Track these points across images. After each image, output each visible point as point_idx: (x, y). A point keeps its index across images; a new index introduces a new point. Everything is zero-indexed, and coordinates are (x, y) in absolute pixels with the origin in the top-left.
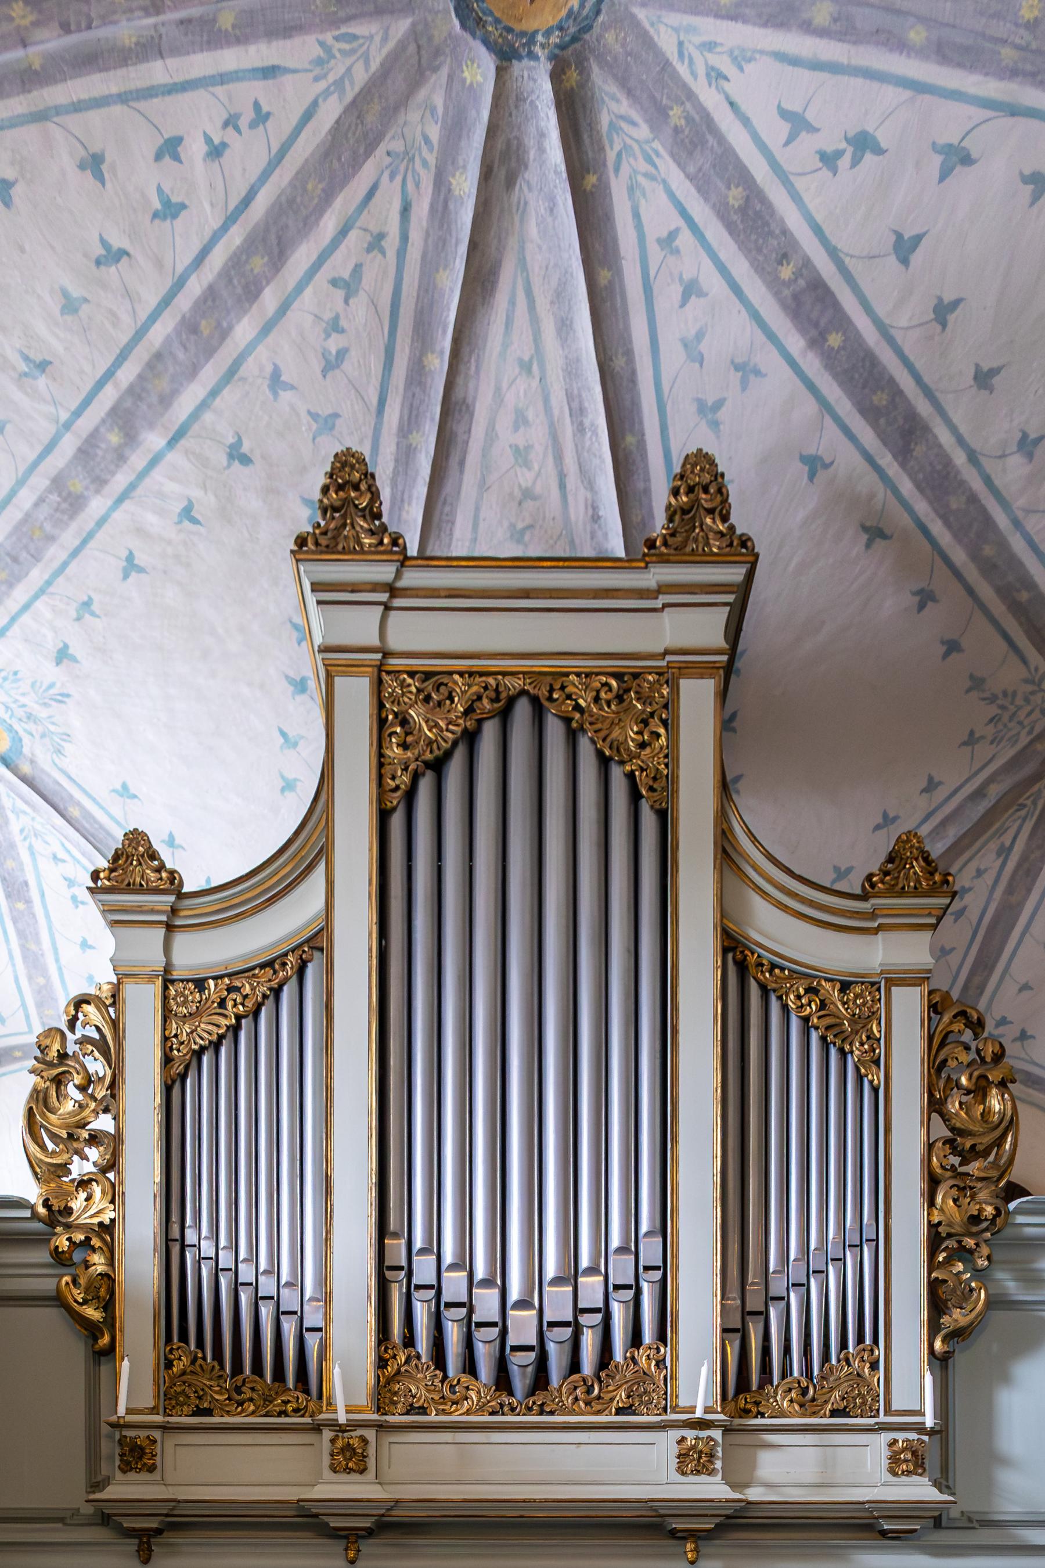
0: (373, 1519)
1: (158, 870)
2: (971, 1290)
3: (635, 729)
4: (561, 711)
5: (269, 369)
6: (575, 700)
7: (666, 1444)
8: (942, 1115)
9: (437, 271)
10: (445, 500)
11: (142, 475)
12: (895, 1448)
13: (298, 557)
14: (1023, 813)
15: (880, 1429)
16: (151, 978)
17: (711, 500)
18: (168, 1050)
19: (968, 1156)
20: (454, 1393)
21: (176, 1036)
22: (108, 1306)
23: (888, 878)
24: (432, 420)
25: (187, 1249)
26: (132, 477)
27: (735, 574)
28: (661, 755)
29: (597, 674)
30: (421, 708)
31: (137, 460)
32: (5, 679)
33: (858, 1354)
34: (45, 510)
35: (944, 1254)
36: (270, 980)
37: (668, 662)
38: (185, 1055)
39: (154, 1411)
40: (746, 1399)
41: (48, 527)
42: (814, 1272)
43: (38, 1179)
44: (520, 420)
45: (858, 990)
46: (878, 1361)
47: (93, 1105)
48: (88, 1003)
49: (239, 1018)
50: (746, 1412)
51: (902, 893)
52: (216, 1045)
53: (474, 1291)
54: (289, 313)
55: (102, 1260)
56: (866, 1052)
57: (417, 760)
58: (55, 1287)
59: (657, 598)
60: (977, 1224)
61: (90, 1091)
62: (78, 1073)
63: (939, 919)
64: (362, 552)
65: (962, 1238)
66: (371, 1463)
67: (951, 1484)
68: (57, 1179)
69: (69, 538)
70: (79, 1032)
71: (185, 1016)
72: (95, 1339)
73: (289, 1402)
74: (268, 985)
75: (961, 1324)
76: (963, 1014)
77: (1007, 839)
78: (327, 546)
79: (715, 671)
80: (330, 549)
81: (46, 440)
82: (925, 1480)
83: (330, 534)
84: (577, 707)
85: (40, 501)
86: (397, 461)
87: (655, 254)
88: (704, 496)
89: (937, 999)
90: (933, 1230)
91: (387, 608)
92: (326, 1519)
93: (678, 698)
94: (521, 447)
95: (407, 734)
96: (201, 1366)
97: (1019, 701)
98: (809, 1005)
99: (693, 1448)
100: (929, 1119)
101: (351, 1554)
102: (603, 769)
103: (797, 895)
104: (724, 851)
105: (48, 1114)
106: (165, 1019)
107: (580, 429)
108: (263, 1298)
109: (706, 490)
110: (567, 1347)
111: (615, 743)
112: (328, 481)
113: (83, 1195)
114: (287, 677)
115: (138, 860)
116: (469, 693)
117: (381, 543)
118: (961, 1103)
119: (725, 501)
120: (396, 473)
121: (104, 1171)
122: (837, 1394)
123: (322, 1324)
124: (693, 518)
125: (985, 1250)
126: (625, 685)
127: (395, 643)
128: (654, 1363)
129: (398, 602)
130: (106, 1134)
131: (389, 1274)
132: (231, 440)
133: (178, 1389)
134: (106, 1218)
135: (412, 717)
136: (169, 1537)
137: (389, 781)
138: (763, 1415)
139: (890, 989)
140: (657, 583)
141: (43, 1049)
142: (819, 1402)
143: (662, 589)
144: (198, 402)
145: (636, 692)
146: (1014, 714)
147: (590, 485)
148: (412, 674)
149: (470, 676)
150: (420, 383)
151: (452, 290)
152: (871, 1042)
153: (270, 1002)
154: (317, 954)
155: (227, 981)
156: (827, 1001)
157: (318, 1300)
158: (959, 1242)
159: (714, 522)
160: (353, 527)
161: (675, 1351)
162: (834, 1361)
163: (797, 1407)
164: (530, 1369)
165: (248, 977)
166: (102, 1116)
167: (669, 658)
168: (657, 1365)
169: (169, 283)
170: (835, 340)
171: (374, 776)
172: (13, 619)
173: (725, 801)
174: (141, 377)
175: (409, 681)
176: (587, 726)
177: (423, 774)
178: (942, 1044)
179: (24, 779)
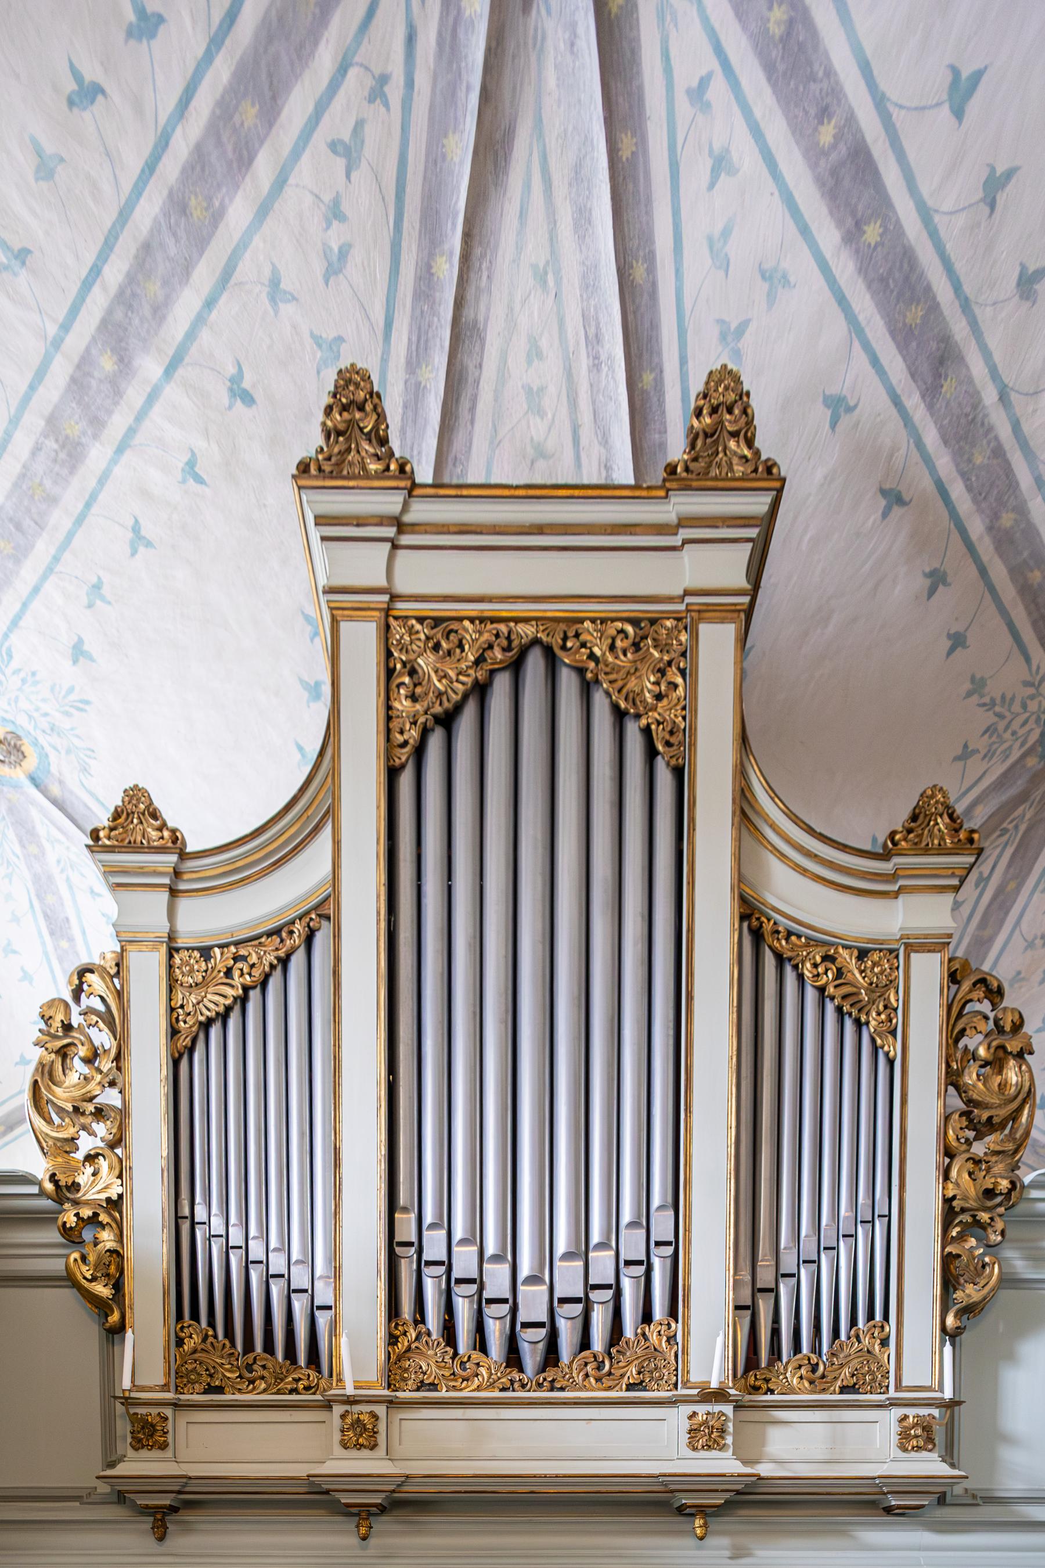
0: (383, 1495)
3: (652, 679)
4: (576, 661)
5: (267, 272)
6: (590, 648)
7: (678, 1419)
8: (957, 1087)
9: (446, 136)
12: (905, 1424)
13: (302, 483)
15: (891, 1405)
16: (156, 943)
17: (736, 421)
18: (174, 1020)
19: (983, 1129)
20: (465, 1369)
21: (182, 1007)
22: (118, 1286)
23: (911, 836)
25: (197, 1226)
26: (130, 420)
27: (757, 504)
29: (613, 620)
30: (431, 657)
31: (135, 395)
33: (868, 1331)
35: (958, 1229)
36: (277, 949)
37: (687, 605)
38: (191, 1027)
39: (165, 1388)
40: (756, 1375)
41: (48, 483)
42: (825, 1248)
43: (44, 1154)
44: (535, 353)
46: (888, 1337)
47: (98, 1077)
48: (92, 971)
49: (246, 989)
50: (756, 1389)
51: (926, 851)
52: (224, 1017)
53: (485, 1266)
54: (286, 188)
56: (882, 1022)
57: (426, 713)
58: (64, 1268)
59: (676, 534)
60: (991, 1199)
61: (96, 1065)
62: (83, 1045)
63: (962, 882)
64: (368, 476)
65: (976, 1213)
66: (381, 1438)
67: (955, 1461)
68: (65, 1155)
69: (72, 499)
71: (191, 986)
72: (107, 1316)
73: (300, 1379)
74: (275, 954)
75: (974, 1299)
76: (983, 981)
78: (332, 472)
79: (735, 615)
80: (331, 476)
82: (934, 1456)
83: (334, 460)
84: (592, 656)
85: (37, 449)
86: (405, 407)
87: (683, 107)
88: (728, 417)
89: (957, 966)
90: (947, 1207)
91: (395, 547)
92: (338, 1495)
94: (535, 389)
95: (415, 685)
96: (212, 1343)
97: (1017, 707)
98: (826, 973)
99: (705, 1423)
100: (946, 1091)
101: (363, 1530)
103: (816, 856)
104: (743, 812)
105: (54, 1087)
106: (171, 989)
109: (730, 411)
110: (579, 1322)
111: (631, 695)
113: (89, 1170)
114: (301, 681)
115: (139, 818)
116: (479, 642)
118: (978, 1075)
119: (750, 423)
121: (112, 1145)
122: (846, 1371)
123: (331, 1303)
124: (716, 442)
125: (999, 1225)
126: (642, 632)
127: (402, 587)
128: (665, 1339)
129: (406, 540)
130: (113, 1108)
131: (399, 1250)
132: (232, 370)
133: (190, 1367)
134: (113, 1193)
135: (419, 665)
137: (398, 736)
138: (772, 1392)
140: (677, 514)
141: (47, 1019)
142: (829, 1379)
144: (193, 316)
145: (654, 640)
147: (605, 441)
148: (421, 620)
149: (481, 623)
151: (462, 162)
152: (888, 1011)
153: (278, 973)
154: (324, 923)
155: (233, 949)
156: (844, 970)
157: (329, 1277)
158: (974, 1216)
159: (738, 446)
160: (358, 452)
162: (843, 1337)
163: (807, 1384)
164: (541, 1346)
165: (255, 946)
167: (688, 600)
168: (668, 1341)
169: (151, 140)
170: (872, 233)
171: (382, 727)
172: (25, 605)
173: (744, 757)
175: (418, 627)
177: (433, 730)
178: (960, 1015)
179: (55, 802)
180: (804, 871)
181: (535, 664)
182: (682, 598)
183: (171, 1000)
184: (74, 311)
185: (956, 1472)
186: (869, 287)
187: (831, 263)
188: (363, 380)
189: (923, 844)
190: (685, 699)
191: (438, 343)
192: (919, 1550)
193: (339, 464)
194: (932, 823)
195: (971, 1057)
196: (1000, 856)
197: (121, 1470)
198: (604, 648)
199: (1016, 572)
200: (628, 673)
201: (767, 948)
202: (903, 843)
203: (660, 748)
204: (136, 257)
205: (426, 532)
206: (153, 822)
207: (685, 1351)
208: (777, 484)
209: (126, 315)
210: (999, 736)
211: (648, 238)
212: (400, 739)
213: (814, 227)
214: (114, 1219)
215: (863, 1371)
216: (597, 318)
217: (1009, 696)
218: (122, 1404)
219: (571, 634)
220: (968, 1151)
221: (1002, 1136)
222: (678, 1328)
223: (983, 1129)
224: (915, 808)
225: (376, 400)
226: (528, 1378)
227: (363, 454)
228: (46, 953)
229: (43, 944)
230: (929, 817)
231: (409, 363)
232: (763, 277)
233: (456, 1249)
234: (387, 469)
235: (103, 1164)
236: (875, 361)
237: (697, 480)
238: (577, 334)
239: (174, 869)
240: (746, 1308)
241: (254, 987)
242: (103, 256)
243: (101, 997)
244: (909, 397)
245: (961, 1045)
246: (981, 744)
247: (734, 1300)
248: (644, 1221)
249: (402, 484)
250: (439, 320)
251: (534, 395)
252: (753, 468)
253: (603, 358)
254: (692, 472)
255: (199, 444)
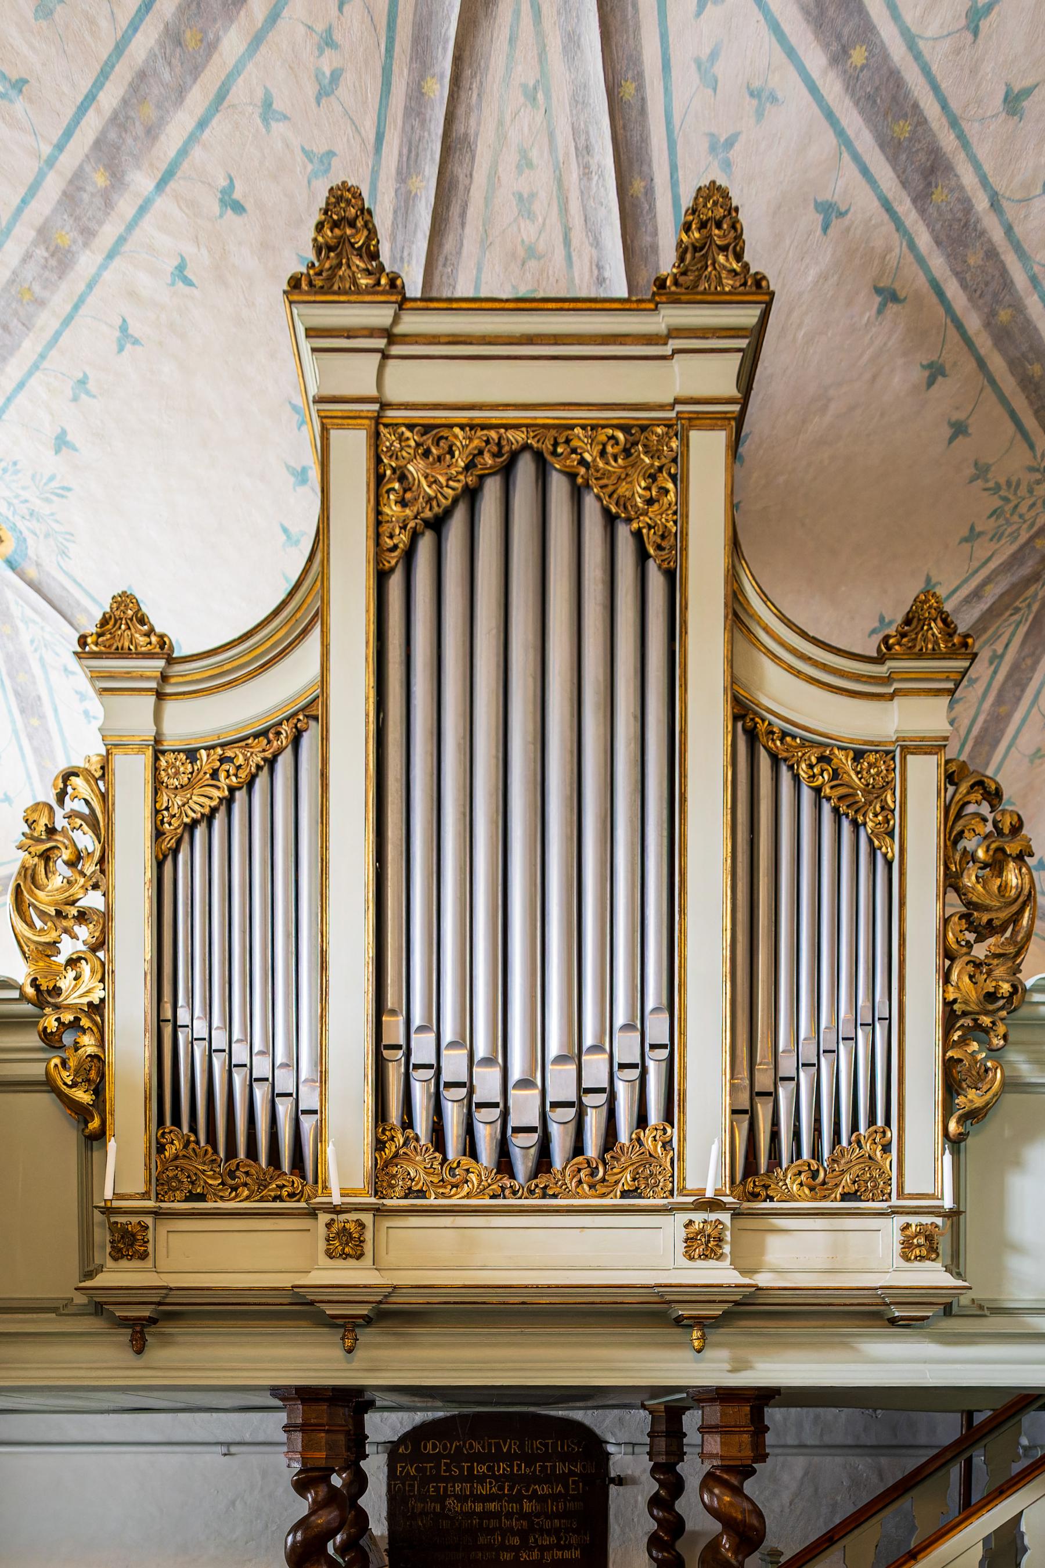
0: (370, 1306)
1: (147, 635)
2: (987, 1070)
3: (643, 484)
4: (566, 467)
5: (259, 94)
6: (581, 454)
7: (674, 1227)
8: (957, 890)
10: (446, 259)
11: (131, 227)
12: (908, 1233)
13: (295, 298)
14: (1017, 617)
15: (893, 1213)
16: (141, 748)
17: (725, 236)
18: (159, 823)
19: (984, 932)
20: (454, 1176)
21: (167, 809)
22: (98, 1091)
23: (905, 640)
24: (432, 159)
25: (180, 1029)
26: (121, 229)
27: (747, 316)
28: (670, 512)
29: (604, 427)
30: (421, 463)
31: (126, 206)
32: (5, 470)
33: (869, 1137)
34: (31, 271)
35: (959, 1033)
36: (264, 751)
37: (678, 413)
38: (176, 829)
39: (145, 1196)
41: (37, 288)
42: (824, 1052)
43: (26, 958)
44: (525, 163)
45: (872, 758)
46: (890, 1143)
47: (82, 881)
48: (77, 775)
49: (232, 790)
50: (754, 1196)
51: (920, 656)
52: (209, 818)
53: (475, 1069)
54: (279, 21)
55: (93, 1042)
57: (416, 518)
59: (666, 344)
61: (79, 867)
63: (957, 686)
64: (359, 291)
66: (368, 1247)
67: (962, 1270)
68: (47, 959)
69: (60, 301)
70: (70, 805)
71: (176, 788)
72: (86, 1123)
73: (284, 1186)
74: (262, 755)
75: (976, 1105)
76: (980, 783)
77: (999, 648)
78: (322, 287)
79: (726, 422)
80: (322, 290)
81: (30, 178)
82: (938, 1265)
83: (324, 274)
84: (582, 462)
85: (27, 257)
88: (717, 232)
89: (954, 768)
90: (948, 1009)
91: (385, 356)
92: (323, 1306)
93: (688, 451)
94: (525, 196)
95: (405, 491)
97: (1023, 491)
98: (822, 774)
99: (701, 1231)
100: (945, 893)
102: (609, 529)
103: (810, 659)
104: (735, 614)
105: (36, 891)
106: (156, 791)
107: (586, 172)
108: (257, 1080)
109: (719, 226)
110: (571, 1128)
112: (323, 217)
113: (71, 974)
114: (288, 467)
115: (127, 624)
117: (378, 283)
118: (977, 877)
119: (739, 237)
120: (394, 224)
121: (94, 949)
122: (848, 1178)
123: (317, 1107)
124: (705, 257)
125: (1001, 1029)
127: (392, 394)
128: (660, 1144)
129: (395, 350)
130: (96, 911)
131: (386, 1053)
132: (223, 183)
133: (171, 1174)
134: (95, 998)
136: (169, 1328)
137: (388, 540)
138: (772, 1199)
139: (905, 758)
141: (31, 824)
143: (674, 333)
144: (185, 135)
145: (645, 446)
146: (1016, 506)
147: (597, 243)
148: (411, 427)
149: (471, 430)
150: (419, 114)
152: (885, 813)
153: (264, 774)
154: (312, 724)
155: (219, 751)
157: (314, 1081)
158: (975, 1020)
159: (727, 260)
160: (349, 267)
161: (682, 1131)
162: (844, 1142)
163: (807, 1191)
164: (533, 1151)
166: (91, 893)
167: (679, 408)
168: (664, 1146)
170: (858, 56)
171: (371, 533)
174: (125, 102)
175: (408, 434)
176: (592, 482)
177: (423, 534)
178: (959, 816)
179: (31, 584)
180: (798, 673)
181: (525, 469)
182: (672, 406)
183: (156, 802)
184: (68, 134)
185: (960, 1283)
186: (857, 103)
187: (817, 83)
188: (354, 197)
189: (918, 648)
190: (676, 504)
191: (429, 157)
192: (925, 1362)
193: (330, 279)
194: (926, 628)
195: (970, 858)
196: (1013, 634)
197: (101, 1280)
198: (595, 454)
199: (1014, 365)
200: (619, 478)
201: (762, 748)
202: (897, 647)
203: (652, 551)
204: (130, 85)
205: (416, 343)
206: (140, 627)
207: (681, 1157)
208: (766, 298)
209: (120, 136)
210: (1007, 520)
211: (636, 60)
212: (390, 543)
213: (800, 51)
214: (95, 1023)
215: (865, 1178)
216: (587, 133)
217: (1014, 479)
218: (103, 1213)
219: (562, 440)
220: (968, 954)
221: (1003, 939)
222: (674, 1133)
223: (984, 932)
224: (908, 613)
225: (367, 217)
226: (520, 1185)
227: (354, 268)
228: (15, 732)
229: (13, 722)
230: (922, 621)
231: (399, 172)
232: (752, 94)
233: (444, 1053)
234: (378, 283)
235: (86, 968)
236: (865, 171)
237: (687, 294)
238: (567, 147)
239: (161, 673)
240: (745, 1112)
241: (240, 788)
242: (99, 84)
243: (86, 800)
244: (901, 202)
245: (960, 846)
246: (989, 525)
247: (731, 1104)
248: (639, 1024)
249: (393, 298)
250: (429, 134)
251: (525, 203)
252: (743, 281)
253: (594, 168)
254: (681, 286)
255: (189, 249)
